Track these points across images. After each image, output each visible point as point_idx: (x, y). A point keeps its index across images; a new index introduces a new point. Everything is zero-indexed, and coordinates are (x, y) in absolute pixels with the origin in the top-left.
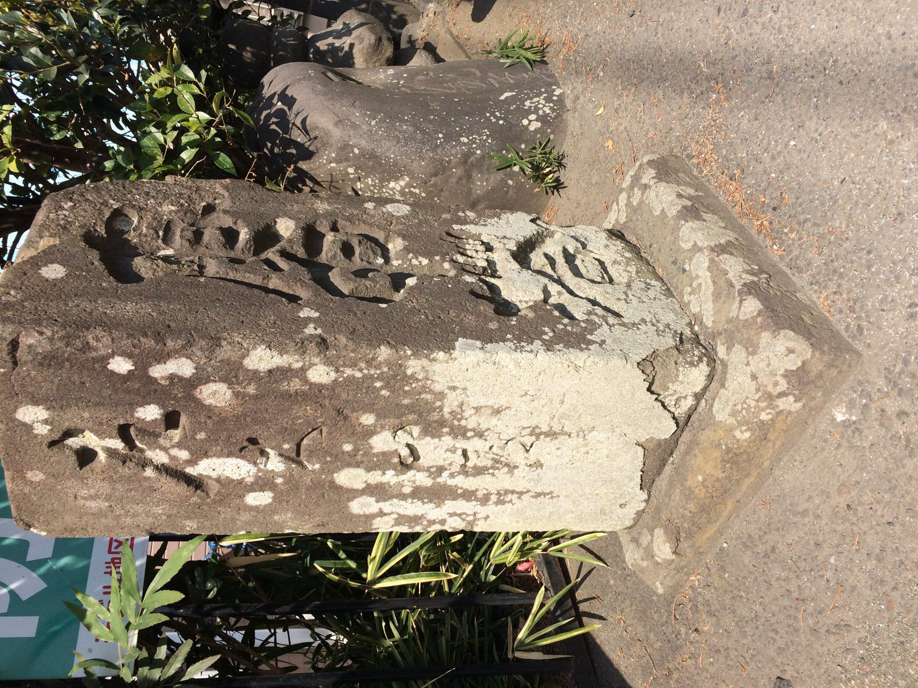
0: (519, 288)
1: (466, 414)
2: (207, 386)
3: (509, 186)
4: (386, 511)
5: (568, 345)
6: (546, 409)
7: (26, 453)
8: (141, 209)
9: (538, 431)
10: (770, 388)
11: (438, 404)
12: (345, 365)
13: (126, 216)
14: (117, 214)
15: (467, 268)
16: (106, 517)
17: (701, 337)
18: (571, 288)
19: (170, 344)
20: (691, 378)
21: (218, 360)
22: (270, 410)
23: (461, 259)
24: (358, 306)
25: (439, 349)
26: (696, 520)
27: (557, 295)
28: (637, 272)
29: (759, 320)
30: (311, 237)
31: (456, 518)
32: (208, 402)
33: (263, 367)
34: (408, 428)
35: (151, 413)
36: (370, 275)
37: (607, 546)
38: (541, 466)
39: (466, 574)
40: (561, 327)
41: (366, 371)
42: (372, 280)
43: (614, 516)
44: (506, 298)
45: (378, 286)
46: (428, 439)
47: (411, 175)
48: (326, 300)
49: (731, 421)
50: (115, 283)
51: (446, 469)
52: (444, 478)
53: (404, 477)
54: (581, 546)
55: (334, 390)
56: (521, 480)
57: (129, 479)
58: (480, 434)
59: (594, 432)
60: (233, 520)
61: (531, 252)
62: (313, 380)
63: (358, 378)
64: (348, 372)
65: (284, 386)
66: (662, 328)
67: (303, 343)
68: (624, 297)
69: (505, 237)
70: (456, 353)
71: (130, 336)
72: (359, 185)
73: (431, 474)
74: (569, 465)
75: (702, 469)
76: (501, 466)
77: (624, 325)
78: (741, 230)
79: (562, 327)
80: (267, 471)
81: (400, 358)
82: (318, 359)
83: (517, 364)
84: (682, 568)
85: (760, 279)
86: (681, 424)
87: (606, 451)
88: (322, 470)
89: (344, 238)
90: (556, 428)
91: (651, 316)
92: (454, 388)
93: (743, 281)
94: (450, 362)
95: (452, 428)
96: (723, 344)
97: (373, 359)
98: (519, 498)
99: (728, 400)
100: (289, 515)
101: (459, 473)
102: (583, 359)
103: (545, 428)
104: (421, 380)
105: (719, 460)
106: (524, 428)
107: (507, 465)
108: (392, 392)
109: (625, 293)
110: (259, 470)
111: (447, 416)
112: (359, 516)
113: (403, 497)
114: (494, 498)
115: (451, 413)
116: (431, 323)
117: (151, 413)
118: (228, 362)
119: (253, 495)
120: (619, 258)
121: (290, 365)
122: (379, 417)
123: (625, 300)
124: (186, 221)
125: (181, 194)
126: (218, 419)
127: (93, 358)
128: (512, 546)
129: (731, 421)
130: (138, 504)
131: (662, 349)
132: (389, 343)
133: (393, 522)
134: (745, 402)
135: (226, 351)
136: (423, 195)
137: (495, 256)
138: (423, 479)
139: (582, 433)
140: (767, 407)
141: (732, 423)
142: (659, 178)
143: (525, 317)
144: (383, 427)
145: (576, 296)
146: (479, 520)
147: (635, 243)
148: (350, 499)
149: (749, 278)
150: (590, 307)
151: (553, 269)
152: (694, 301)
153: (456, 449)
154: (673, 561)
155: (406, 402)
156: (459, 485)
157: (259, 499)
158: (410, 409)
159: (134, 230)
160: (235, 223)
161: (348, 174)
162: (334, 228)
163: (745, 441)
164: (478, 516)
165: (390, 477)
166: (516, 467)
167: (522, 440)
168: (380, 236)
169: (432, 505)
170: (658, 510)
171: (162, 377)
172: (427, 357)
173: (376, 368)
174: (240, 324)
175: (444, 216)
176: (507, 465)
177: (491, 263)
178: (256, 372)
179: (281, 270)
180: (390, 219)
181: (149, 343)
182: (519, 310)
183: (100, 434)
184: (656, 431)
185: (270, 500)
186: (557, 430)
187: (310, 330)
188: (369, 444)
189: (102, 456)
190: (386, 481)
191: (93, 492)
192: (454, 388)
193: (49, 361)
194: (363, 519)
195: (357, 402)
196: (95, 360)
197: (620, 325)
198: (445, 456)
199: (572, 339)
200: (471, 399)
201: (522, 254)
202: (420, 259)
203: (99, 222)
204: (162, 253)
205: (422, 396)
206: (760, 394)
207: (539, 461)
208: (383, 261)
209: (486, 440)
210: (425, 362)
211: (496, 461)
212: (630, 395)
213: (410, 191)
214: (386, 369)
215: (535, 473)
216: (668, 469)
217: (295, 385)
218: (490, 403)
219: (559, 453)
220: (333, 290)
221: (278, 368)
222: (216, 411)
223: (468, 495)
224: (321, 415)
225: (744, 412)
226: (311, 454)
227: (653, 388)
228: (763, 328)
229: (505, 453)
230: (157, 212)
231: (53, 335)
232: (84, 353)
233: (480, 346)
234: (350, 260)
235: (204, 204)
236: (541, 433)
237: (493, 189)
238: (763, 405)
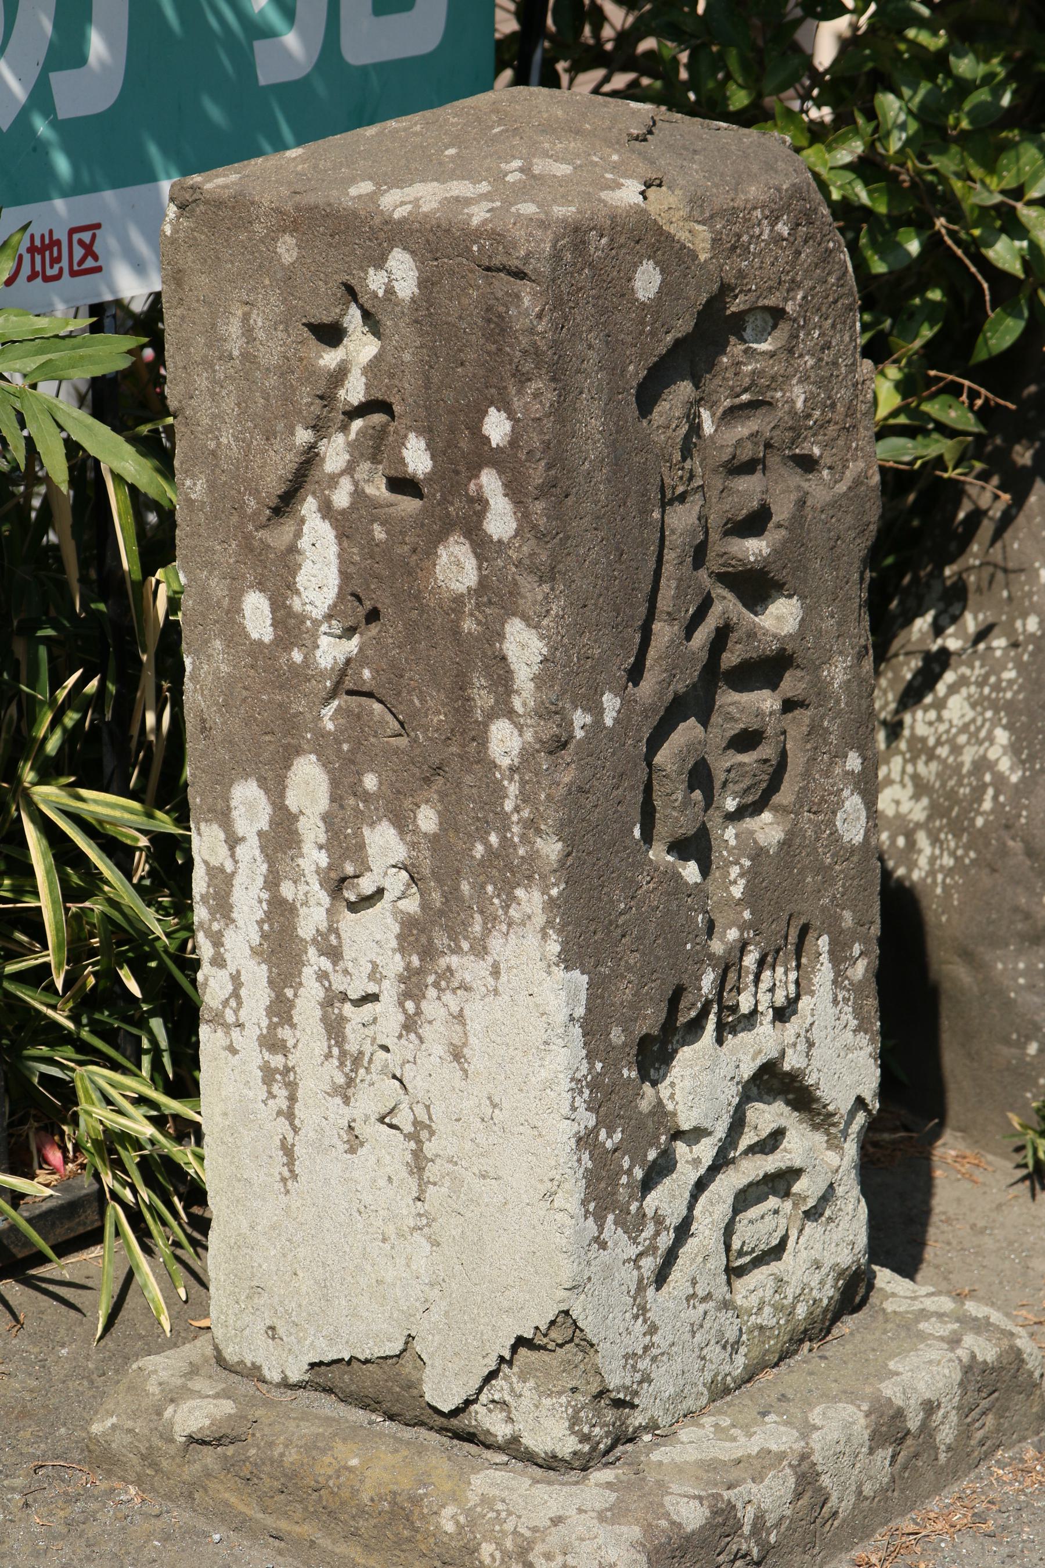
0: (700, 1081)
1: (448, 997)
2: (471, 555)
3: (1023, 1046)
4: (239, 850)
5: (592, 1178)
6: (468, 1145)
7: (330, 245)
8: (791, 351)
9: (424, 1135)
10: (539, 1548)
11: (465, 946)
12: (523, 783)
13: (775, 327)
14: (777, 314)
15: (732, 976)
16: (210, 346)
17: (629, 1447)
18: (712, 1187)
19: (539, 506)
20: (548, 1423)
21: (517, 577)
22: (433, 652)
23: (750, 960)
24: (632, 788)
25: (565, 944)
26: (267, 1469)
27: (692, 1159)
28: (761, 1328)
29: (664, 1523)
30: (768, 669)
31: (230, 988)
32: (441, 550)
33: (511, 648)
34: (415, 889)
35: (417, 458)
36: (698, 795)
37: (141, 1337)
38: (352, 1150)
39: (50, 1012)
40: (626, 1163)
41: (515, 818)
42: (686, 803)
43: (247, 1318)
44: (680, 1055)
45: (676, 813)
46: (396, 929)
47: (1026, 787)
48: (638, 730)
49: (473, 1499)
50: (634, 384)
51: (335, 964)
52: (315, 960)
53: (316, 886)
54: (130, 1276)
55: (478, 762)
56: (321, 1111)
57: (288, 397)
58: (410, 1025)
59: (428, 1247)
60: (211, 566)
61: (788, 1103)
62: (493, 728)
63: (502, 805)
64: (513, 789)
65: (479, 680)
66: (641, 1365)
67: (556, 713)
68: (701, 1293)
69: (811, 1044)
70: (559, 973)
71: (547, 445)
72: (999, 643)
73: (325, 936)
74: (356, 1205)
75: (375, 1460)
76: (347, 1070)
77: (641, 1288)
78: (859, 1529)
79: (626, 1166)
80: (315, 637)
81: (543, 877)
82: (531, 740)
83: (549, 1085)
84: (155, 1465)
85: (747, 1539)
86: (455, 1422)
87: (389, 1276)
88: (323, 734)
89: (769, 732)
90: (432, 1171)
91: (664, 1345)
92: (496, 973)
93: (739, 1505)
94: (544, 964)
95: (420, 972)
96: (617, 1477)
97: (538, 831)
98: (279, 1113)
99: (512, 1490)
100: (225, 668)
101: (328, 990)
102: (568, 1206)
103: (430, 1148)
104: (506, 913)
105: (395, 1488)
106: (428, 1107)
107: (350, 1082)
108: (481, 863)
109: (708, 1297)
110: (317, 623)
111: (443, 962)
112: (227, 799)
113: (272, 883)
114: (277, 1061)
115: (449, 969)
116: (611, 923)
117: (417, 458)
118: (515, 591)
119: (268, 605)
120: (790, 1292)
121: (518, 692)
122: (434, 839)
123: (694, 1295)
124: (776, 433)
125: (833, 406)
126: (413, 564)
127: (505, 388)
128: (120, 1112)
129: (473, 1499)
130: (238, 405)
131: (599, 1360)
132: (569, 854)
133: (214, 862)
134: (510, 1513)
135: (533, 591)
136: (980, 822)
137: (765, 1027)
138: (312, 919)
139: (425, 1223)
140: (505, 1553)
141: (468, 1500)
142: (971, 1368)
143: (639, 1094)
144: (413, 846)
145: (694, 1198)
146: (227, 1034)
147: (835, 1332)
148: (262, 783)
149: (747, 1516)
150: (673, 1220)
151: (752, 1150)
152: (701, 1432)
153: (379, 982)
154: (172, 1441)
155: (465, 887)
156: (302, 991)
157: (257, 615)
158: (452, 895)
159: (746, 351)
160: (779, 526)
161: (1024, 616)
162: (789, 705)
163: (438, 1526)
164: (235, 1033)
165: (314, 857)
166: (347, 1101)
167: (404, 1106)
168: (785, 796)
169: (256, 939)
170: (267, 1403)
171: (481, 487)
172: (549, 923)
173: (523, 837)
174: (581, 603)
175: (847, 915)
176: (350, 1082)
177: (751, 1019)
178: (501, 636)
179: (689, 637)
180: (827, 807)
181: (537, 474)
182: (654, 1084)
183: (372, 368)
184: (439, 1370)
185: (255, 636)
186: (427, 1174)
187: (580, 718)
188: (380, 820)
189: (330, 358)
190: (305, 850)
191: (261, 335)
192: (496, 973)
193: (496, 325)
194: (220, 805)
195: (458, 801)
196: (502, 390)
197: (640, 1280)
198: (363, 961)
199: (603, 1185)
200: (478, 1005)
201: (773, 1081)
202: (742, 882)
203: (751, 297)
204: (705, 414)
205: (478, 917)
206: (528, 1534)
207: (362, 1144)
208: (732, 809)
209: (400, 1037)
210: (540, 919)
211: (357, 1060)
212: (506, 1304)
213: (984, 787)
214: (521, 852)
215: (335, 1141)
216: (360, 1416)
217: (483, 699)
218: (472, 1040)
219: (382, 1182)
220: (656, 742)
221: (509, 672)
222: (427, 564)
223: (281, 1010)
224: (431, 739)
225: (492, 1515)
226: (353, 718)
227: (523, 1351)
228: (648, 1529)
229: (374, 1077)
230: (787, 378)
231: (538, 334)
232: (514, 375)
233: (576, 1015)
234: (726, 749)
235: (816, 451)
236: (419, 1142)
237: (1009, 1005)
238: (509, 1544)
